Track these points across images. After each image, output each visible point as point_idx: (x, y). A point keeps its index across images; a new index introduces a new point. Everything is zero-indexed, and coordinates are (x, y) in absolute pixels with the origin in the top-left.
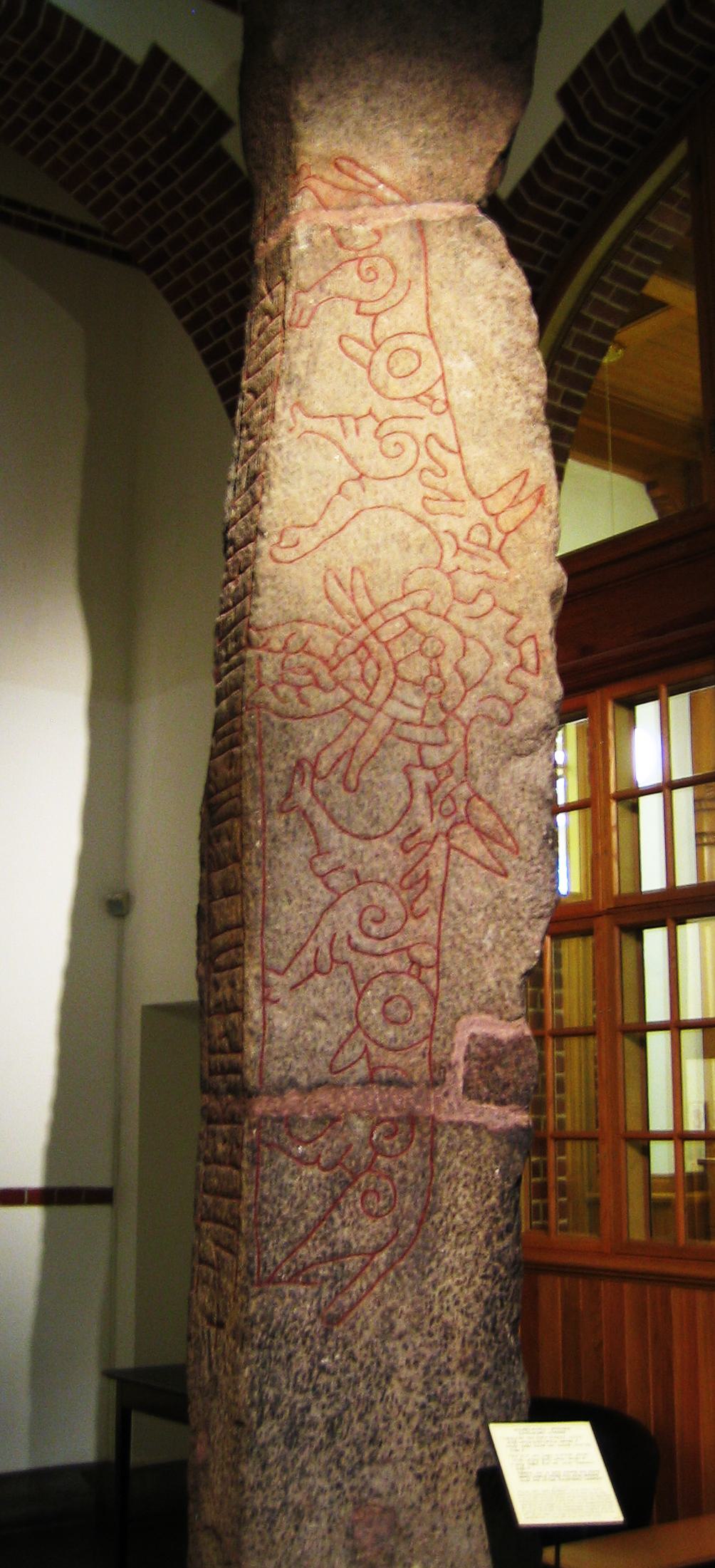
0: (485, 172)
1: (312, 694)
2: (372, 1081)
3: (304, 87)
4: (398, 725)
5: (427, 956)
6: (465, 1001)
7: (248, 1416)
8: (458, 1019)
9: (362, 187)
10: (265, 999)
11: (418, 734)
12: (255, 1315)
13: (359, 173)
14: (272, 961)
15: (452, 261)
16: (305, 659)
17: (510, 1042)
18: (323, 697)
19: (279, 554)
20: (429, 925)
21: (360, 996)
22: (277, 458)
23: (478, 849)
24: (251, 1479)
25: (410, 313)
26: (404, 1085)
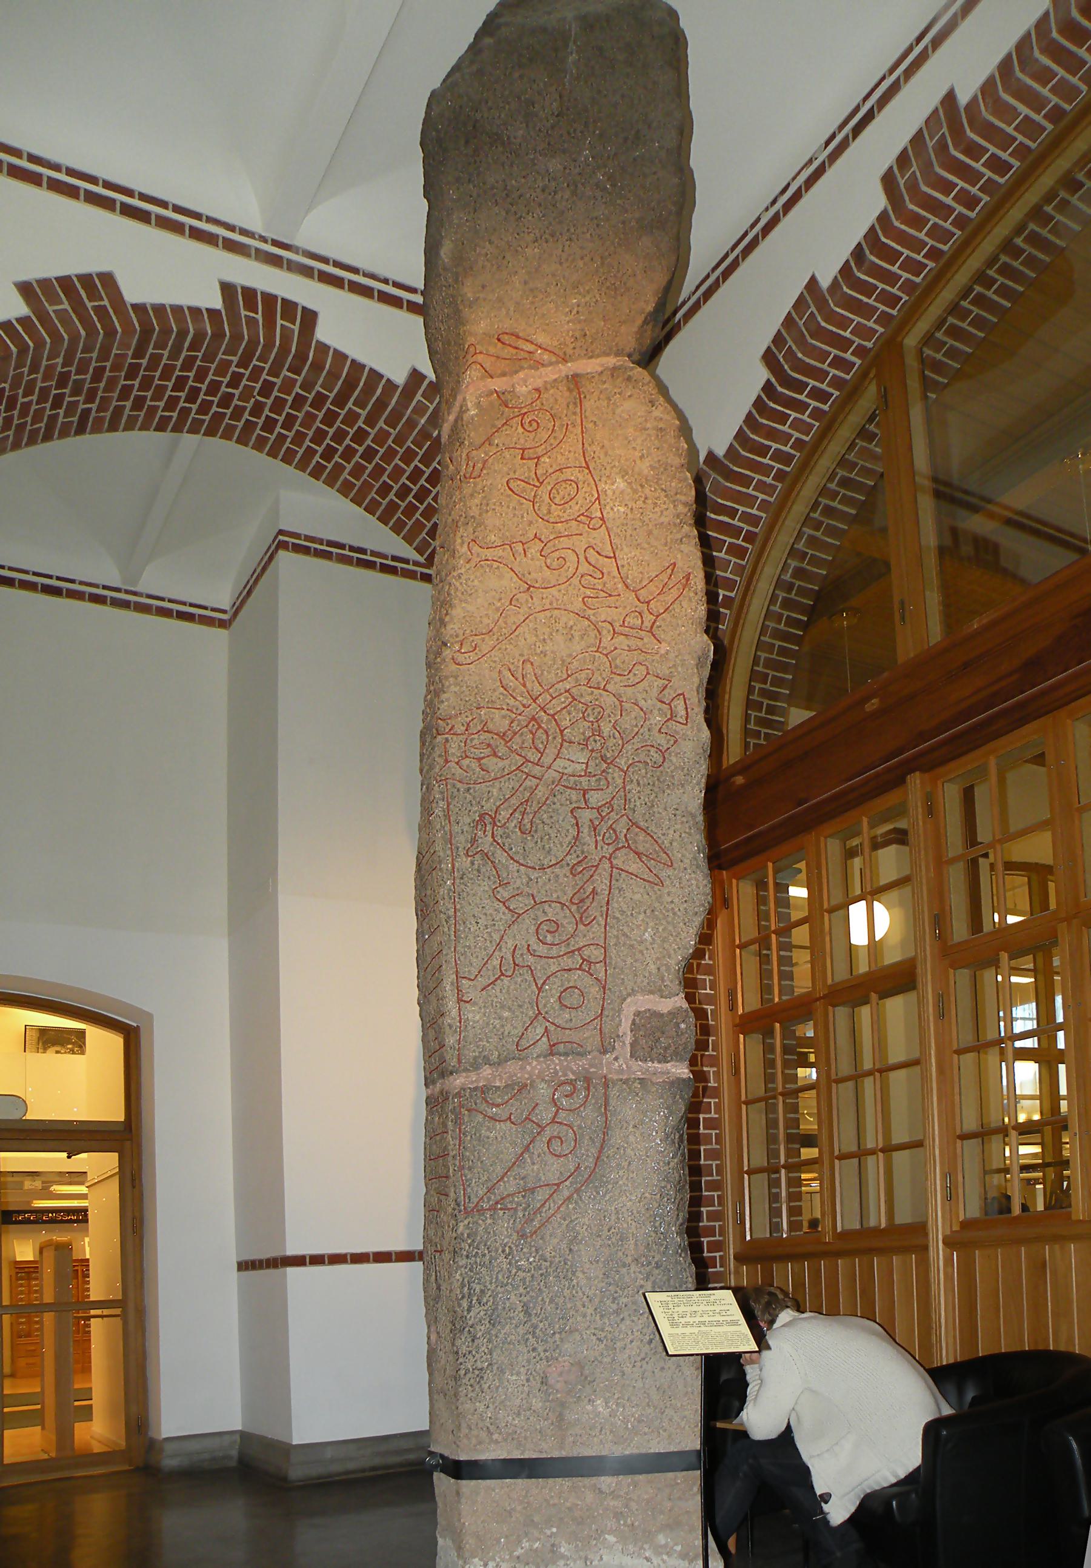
0: (635, 329)
1: (491, 763)
2: (552, 1054)
3: (468, 282)
4: (565, 777)
5: (596, 954)
6: (630, 985)
7: (460, 1305)
8: (625, 999)
9: (523, 355)
10: (460, 1000)
11: (584, 782)
12: (462, 1234)
13: (521, 344)
14: (464, 970)
15: (605, 403)
16: (484, 736)
17: (670, 1013)
18: (501, 764)
19: (460, 658)
20: (597, 929)
21: (540, 990)
22: (458, 584)
23: (634, 866)
24: (464, 1349)
25: (569, 451)
26: (580, 1053)
